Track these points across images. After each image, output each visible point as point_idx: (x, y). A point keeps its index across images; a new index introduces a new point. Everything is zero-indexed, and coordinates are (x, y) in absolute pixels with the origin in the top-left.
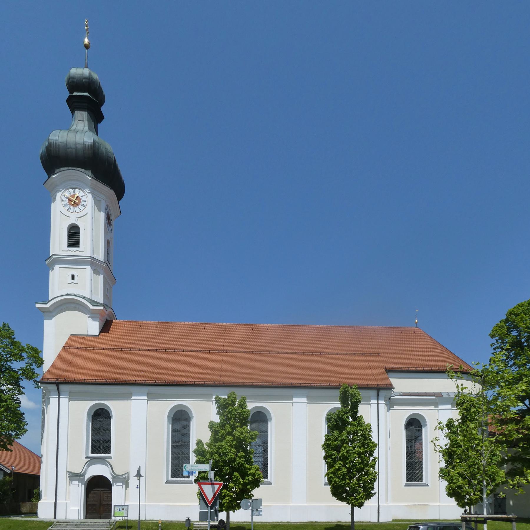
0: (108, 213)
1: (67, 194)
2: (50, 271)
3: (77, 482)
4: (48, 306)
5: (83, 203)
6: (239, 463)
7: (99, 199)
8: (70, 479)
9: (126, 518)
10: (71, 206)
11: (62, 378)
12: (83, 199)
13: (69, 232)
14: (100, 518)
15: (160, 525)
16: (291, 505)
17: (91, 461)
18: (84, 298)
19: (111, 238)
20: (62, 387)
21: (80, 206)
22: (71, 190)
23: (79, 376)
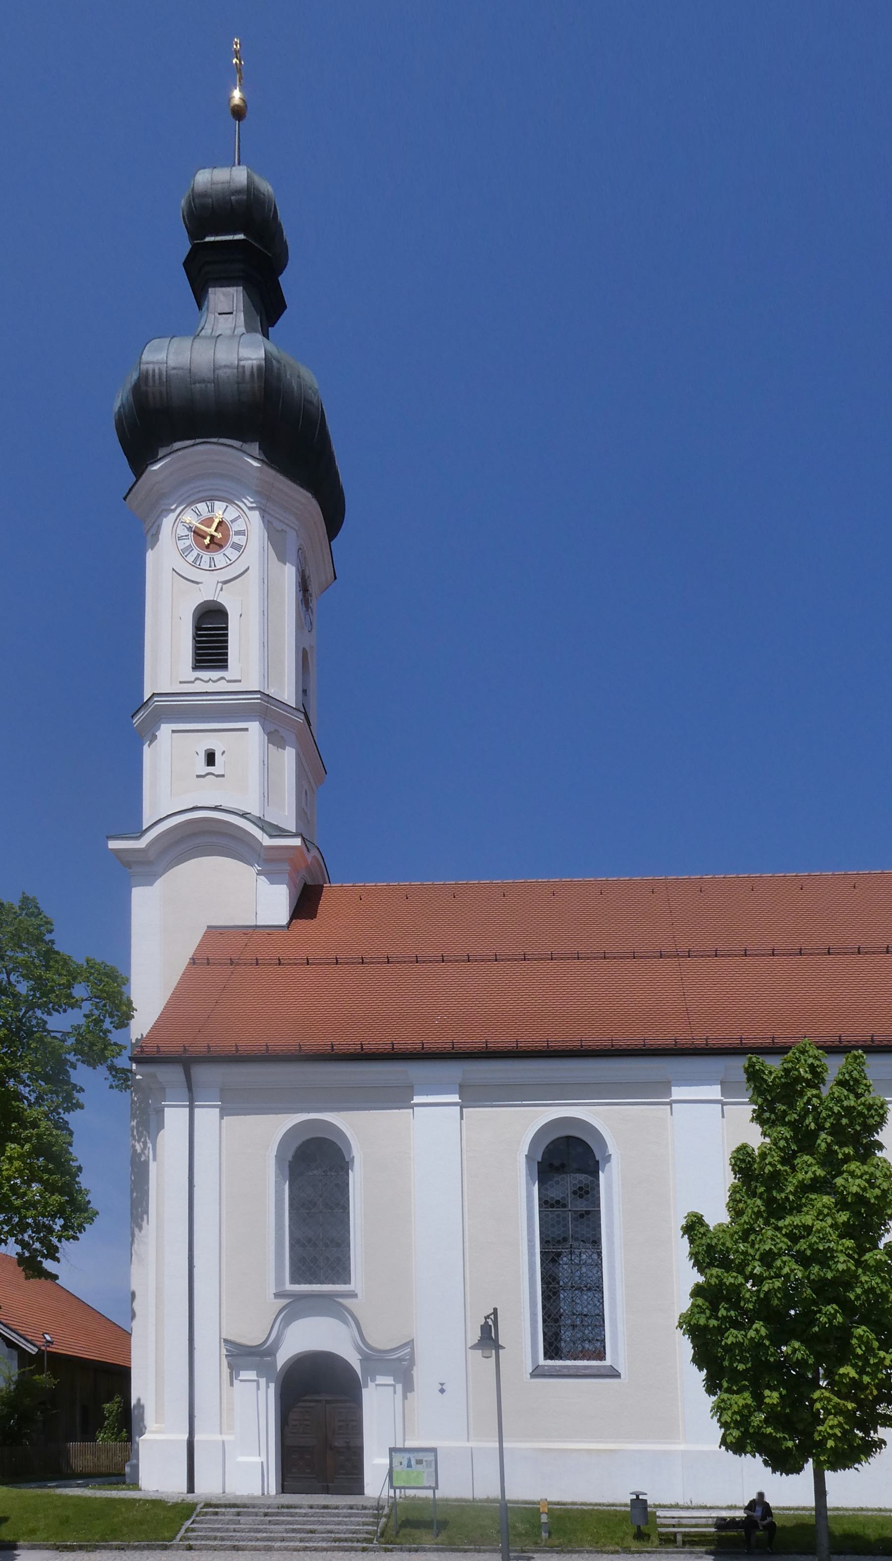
0: (303, 571)
1: (190, 518)
2: (146, 747)
3: (251, 1375)
4: (142, 843)
5: (235, 539)
6: (872, 1289)
7: (280, 526)
8: (230, 1366)
9: (429, 1493)
10: (202, 553)
11: (199, 1046)
12: (235, 527)
13: (198, 628)
14: (327, 1491)
15: (544, 1519)
16: (682, 1447)
17: (295, 1308)
18: (244, 815)
19: (311, 647)
20: (201, 1073)
21: (228, 551)
22: (202, 507)
23: (251, 1039)
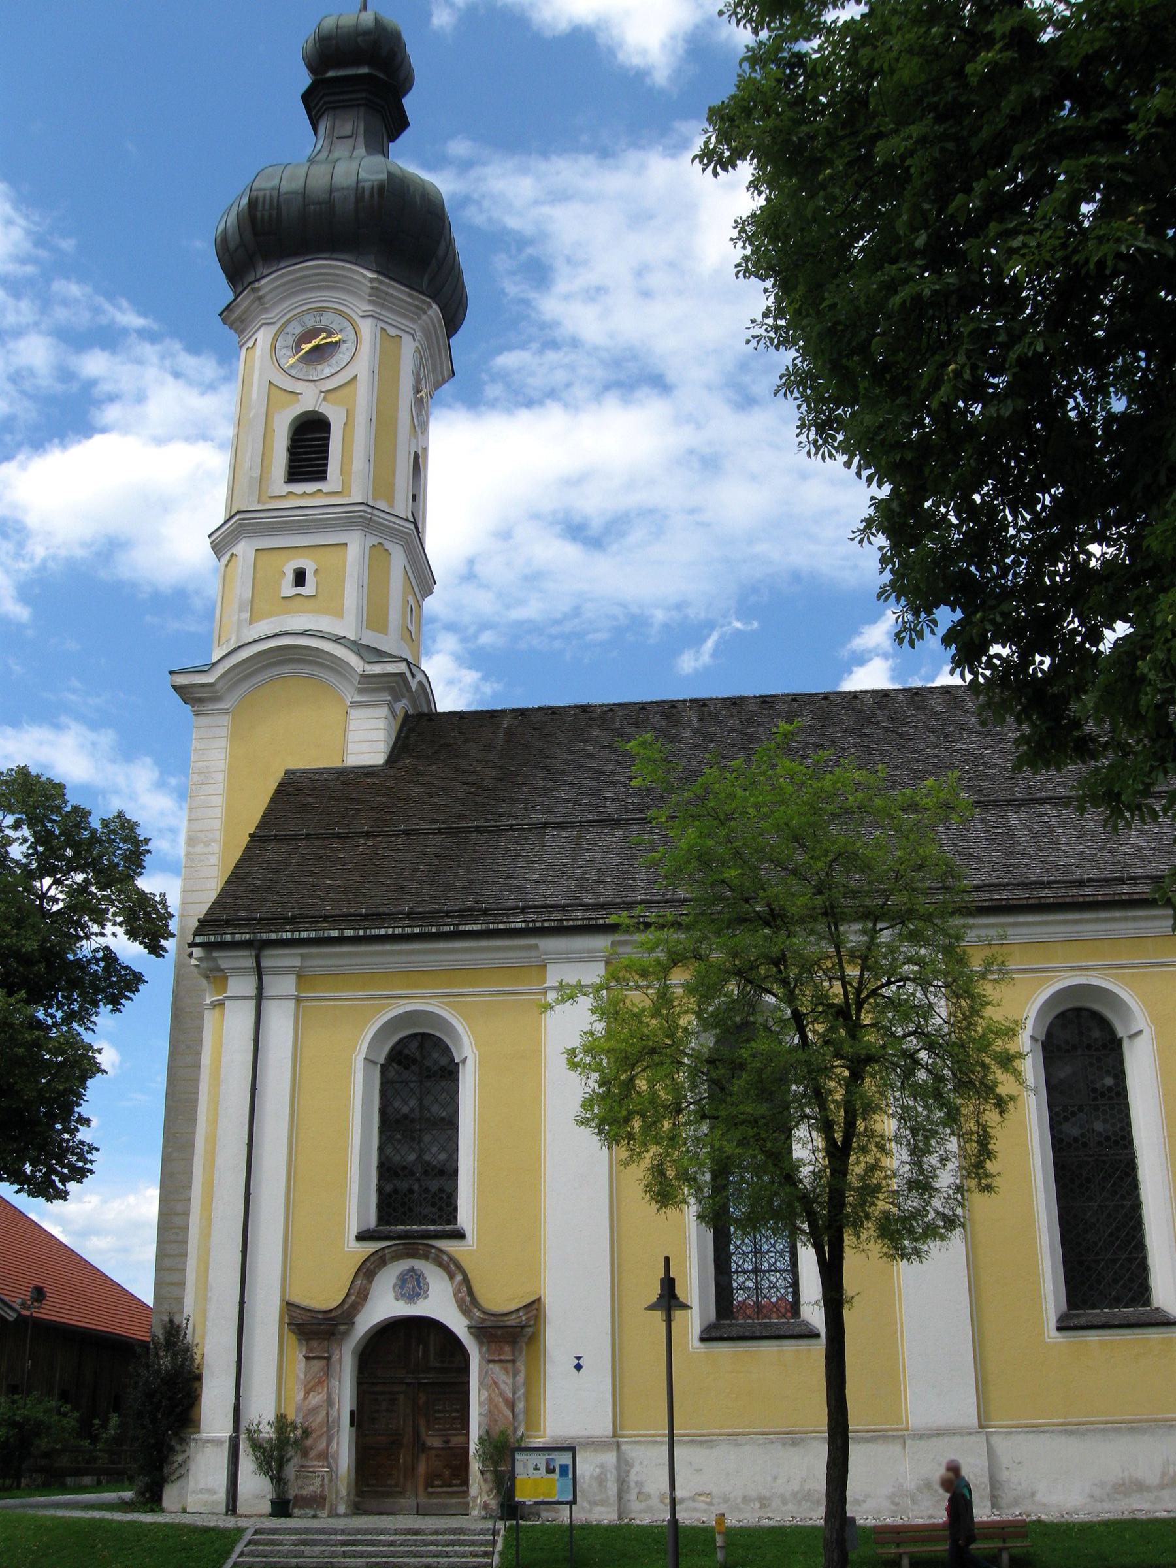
7: (393, 332)
18: (338, 640)
